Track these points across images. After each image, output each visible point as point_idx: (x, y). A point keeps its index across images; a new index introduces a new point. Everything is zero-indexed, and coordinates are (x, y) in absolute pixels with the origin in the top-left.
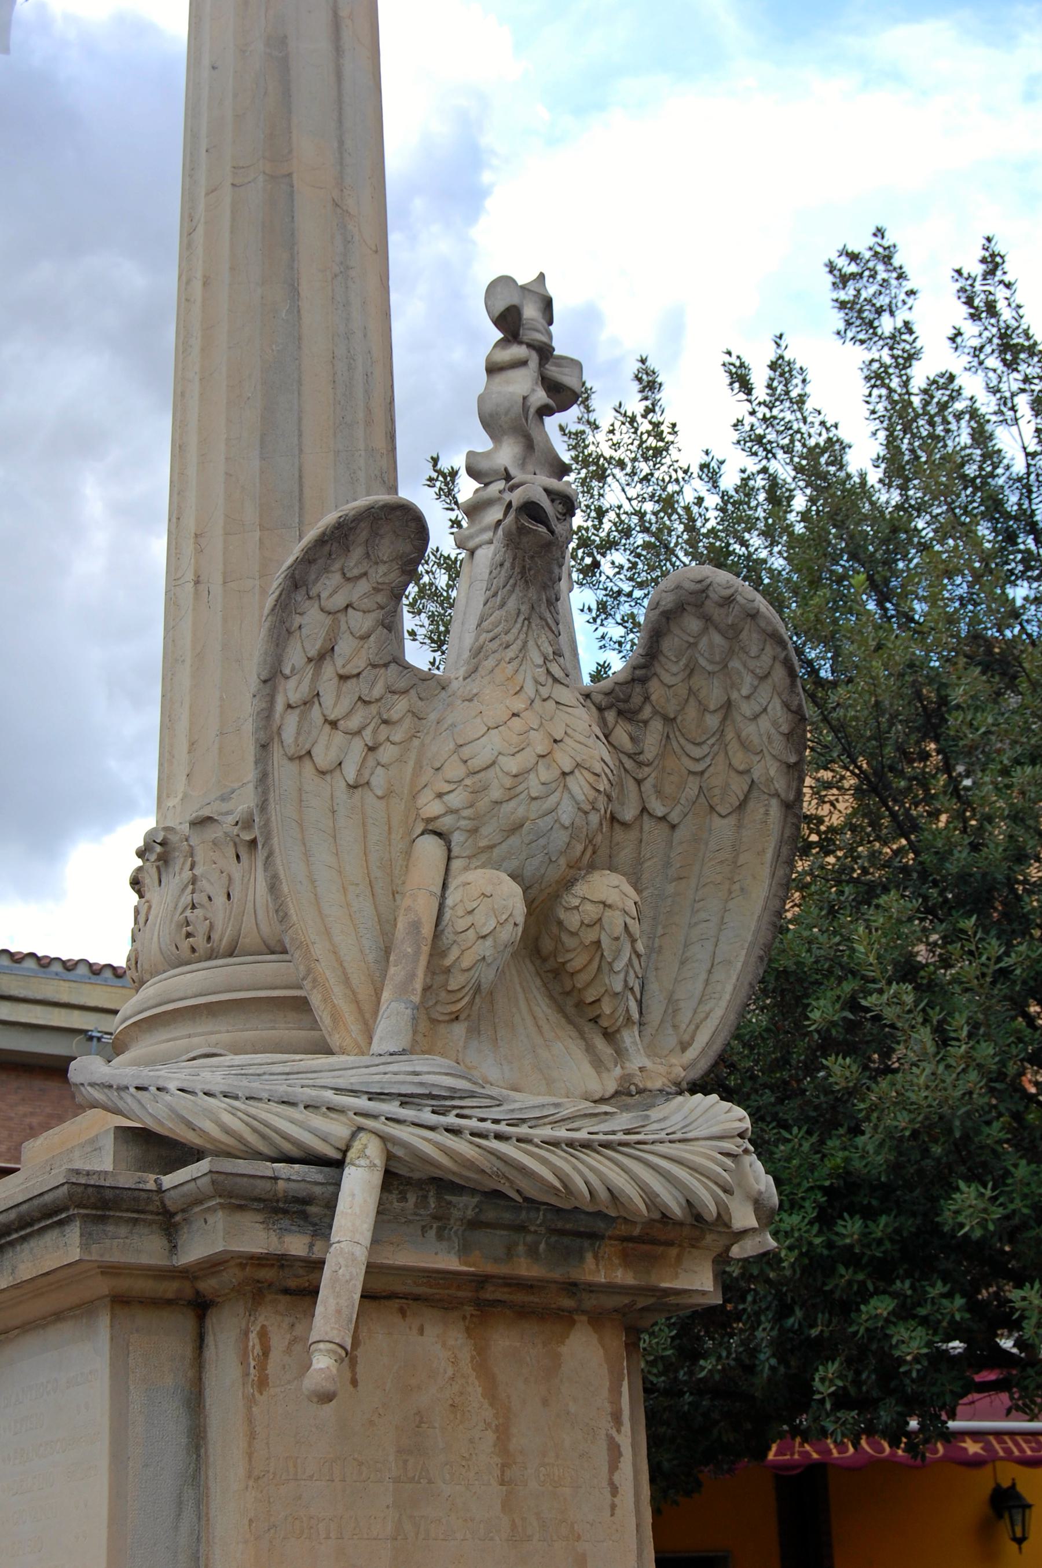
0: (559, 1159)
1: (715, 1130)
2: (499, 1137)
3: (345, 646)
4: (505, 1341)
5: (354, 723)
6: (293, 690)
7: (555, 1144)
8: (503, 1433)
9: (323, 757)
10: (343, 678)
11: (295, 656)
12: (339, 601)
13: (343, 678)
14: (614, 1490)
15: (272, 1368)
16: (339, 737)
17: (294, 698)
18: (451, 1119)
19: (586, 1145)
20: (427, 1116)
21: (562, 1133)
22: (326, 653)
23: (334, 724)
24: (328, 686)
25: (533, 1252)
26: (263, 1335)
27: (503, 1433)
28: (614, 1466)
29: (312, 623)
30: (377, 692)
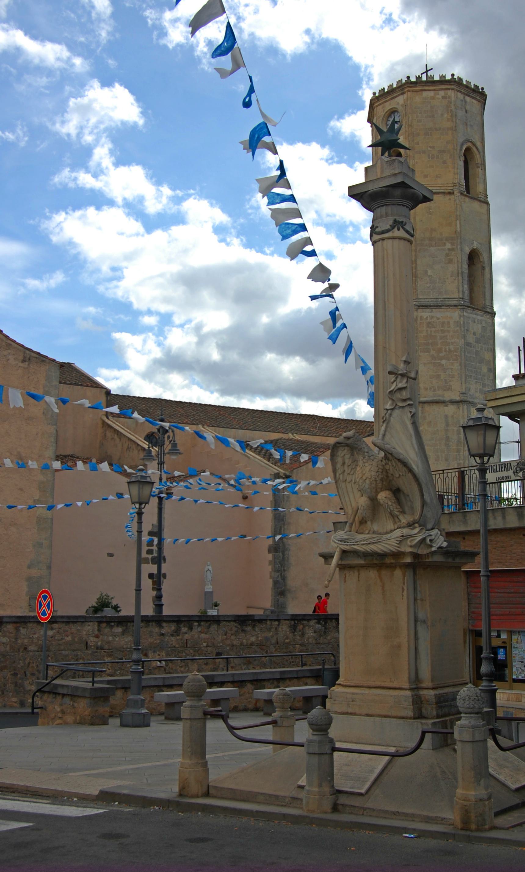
0: (364, 547)
1: (395, 536)
2: (354, 545)
3: (347, 461)
4: (384, 572)
5: (352, 473)
6: (339, 472)
7: (364, 544)
8: (383, 587)
9: (348, 480)
10: (348, 466)
11: (339, 466)
12: (342, 455)
13: (348, 466)
14: (403, 596)
15: (347, 579)
16: (350, 476)
17: (340, 472)
18: (346, 543)
19: (369, 544)
20: (343, 543)
21: (365, 542)
22: (344, 464)
23: (349, 474)
24: (346, 468)
25: (376, 559)
26: (345, 574)
27: (383, 587)
28: (403, 592)
29: (339, 460)
30: (354, 467)
